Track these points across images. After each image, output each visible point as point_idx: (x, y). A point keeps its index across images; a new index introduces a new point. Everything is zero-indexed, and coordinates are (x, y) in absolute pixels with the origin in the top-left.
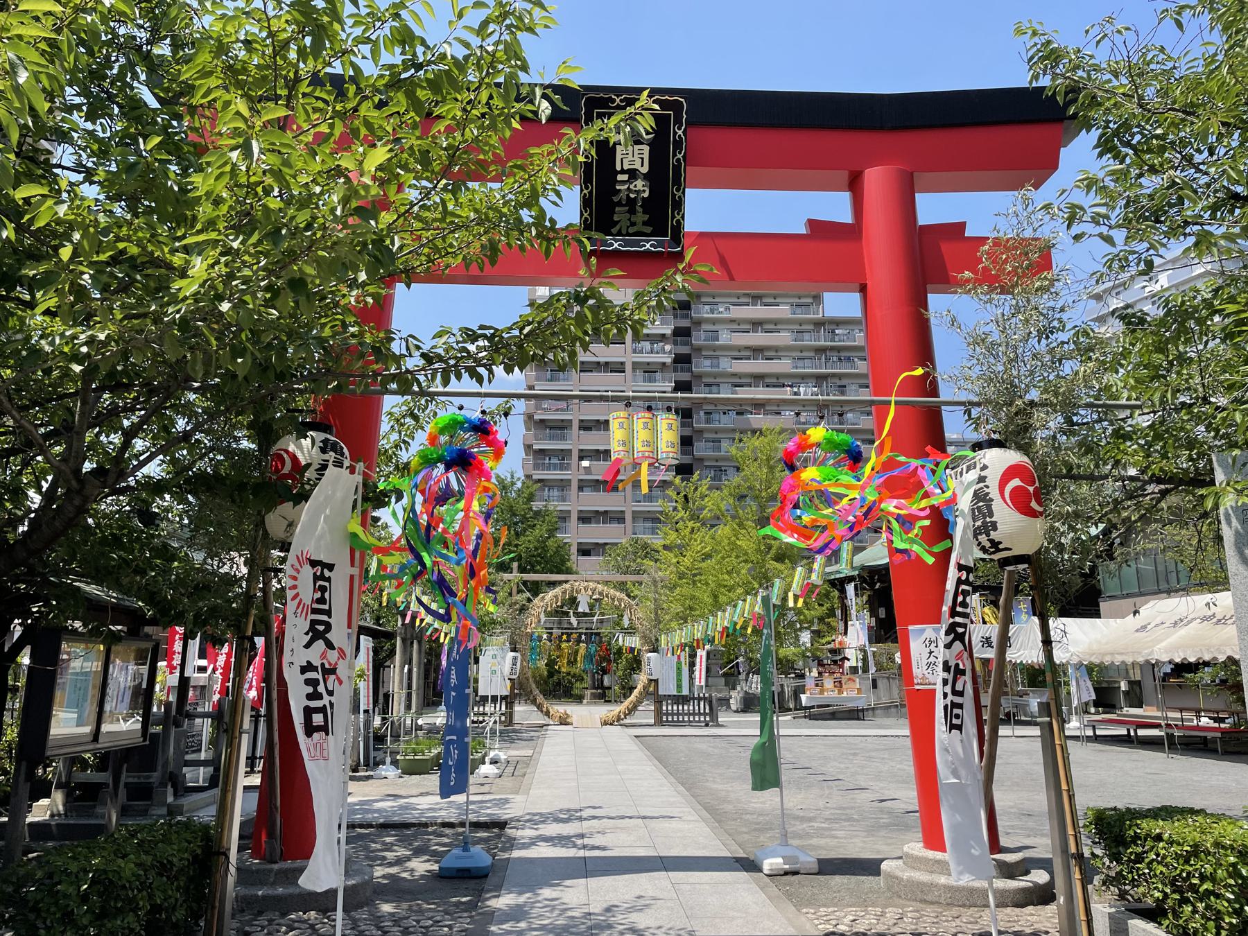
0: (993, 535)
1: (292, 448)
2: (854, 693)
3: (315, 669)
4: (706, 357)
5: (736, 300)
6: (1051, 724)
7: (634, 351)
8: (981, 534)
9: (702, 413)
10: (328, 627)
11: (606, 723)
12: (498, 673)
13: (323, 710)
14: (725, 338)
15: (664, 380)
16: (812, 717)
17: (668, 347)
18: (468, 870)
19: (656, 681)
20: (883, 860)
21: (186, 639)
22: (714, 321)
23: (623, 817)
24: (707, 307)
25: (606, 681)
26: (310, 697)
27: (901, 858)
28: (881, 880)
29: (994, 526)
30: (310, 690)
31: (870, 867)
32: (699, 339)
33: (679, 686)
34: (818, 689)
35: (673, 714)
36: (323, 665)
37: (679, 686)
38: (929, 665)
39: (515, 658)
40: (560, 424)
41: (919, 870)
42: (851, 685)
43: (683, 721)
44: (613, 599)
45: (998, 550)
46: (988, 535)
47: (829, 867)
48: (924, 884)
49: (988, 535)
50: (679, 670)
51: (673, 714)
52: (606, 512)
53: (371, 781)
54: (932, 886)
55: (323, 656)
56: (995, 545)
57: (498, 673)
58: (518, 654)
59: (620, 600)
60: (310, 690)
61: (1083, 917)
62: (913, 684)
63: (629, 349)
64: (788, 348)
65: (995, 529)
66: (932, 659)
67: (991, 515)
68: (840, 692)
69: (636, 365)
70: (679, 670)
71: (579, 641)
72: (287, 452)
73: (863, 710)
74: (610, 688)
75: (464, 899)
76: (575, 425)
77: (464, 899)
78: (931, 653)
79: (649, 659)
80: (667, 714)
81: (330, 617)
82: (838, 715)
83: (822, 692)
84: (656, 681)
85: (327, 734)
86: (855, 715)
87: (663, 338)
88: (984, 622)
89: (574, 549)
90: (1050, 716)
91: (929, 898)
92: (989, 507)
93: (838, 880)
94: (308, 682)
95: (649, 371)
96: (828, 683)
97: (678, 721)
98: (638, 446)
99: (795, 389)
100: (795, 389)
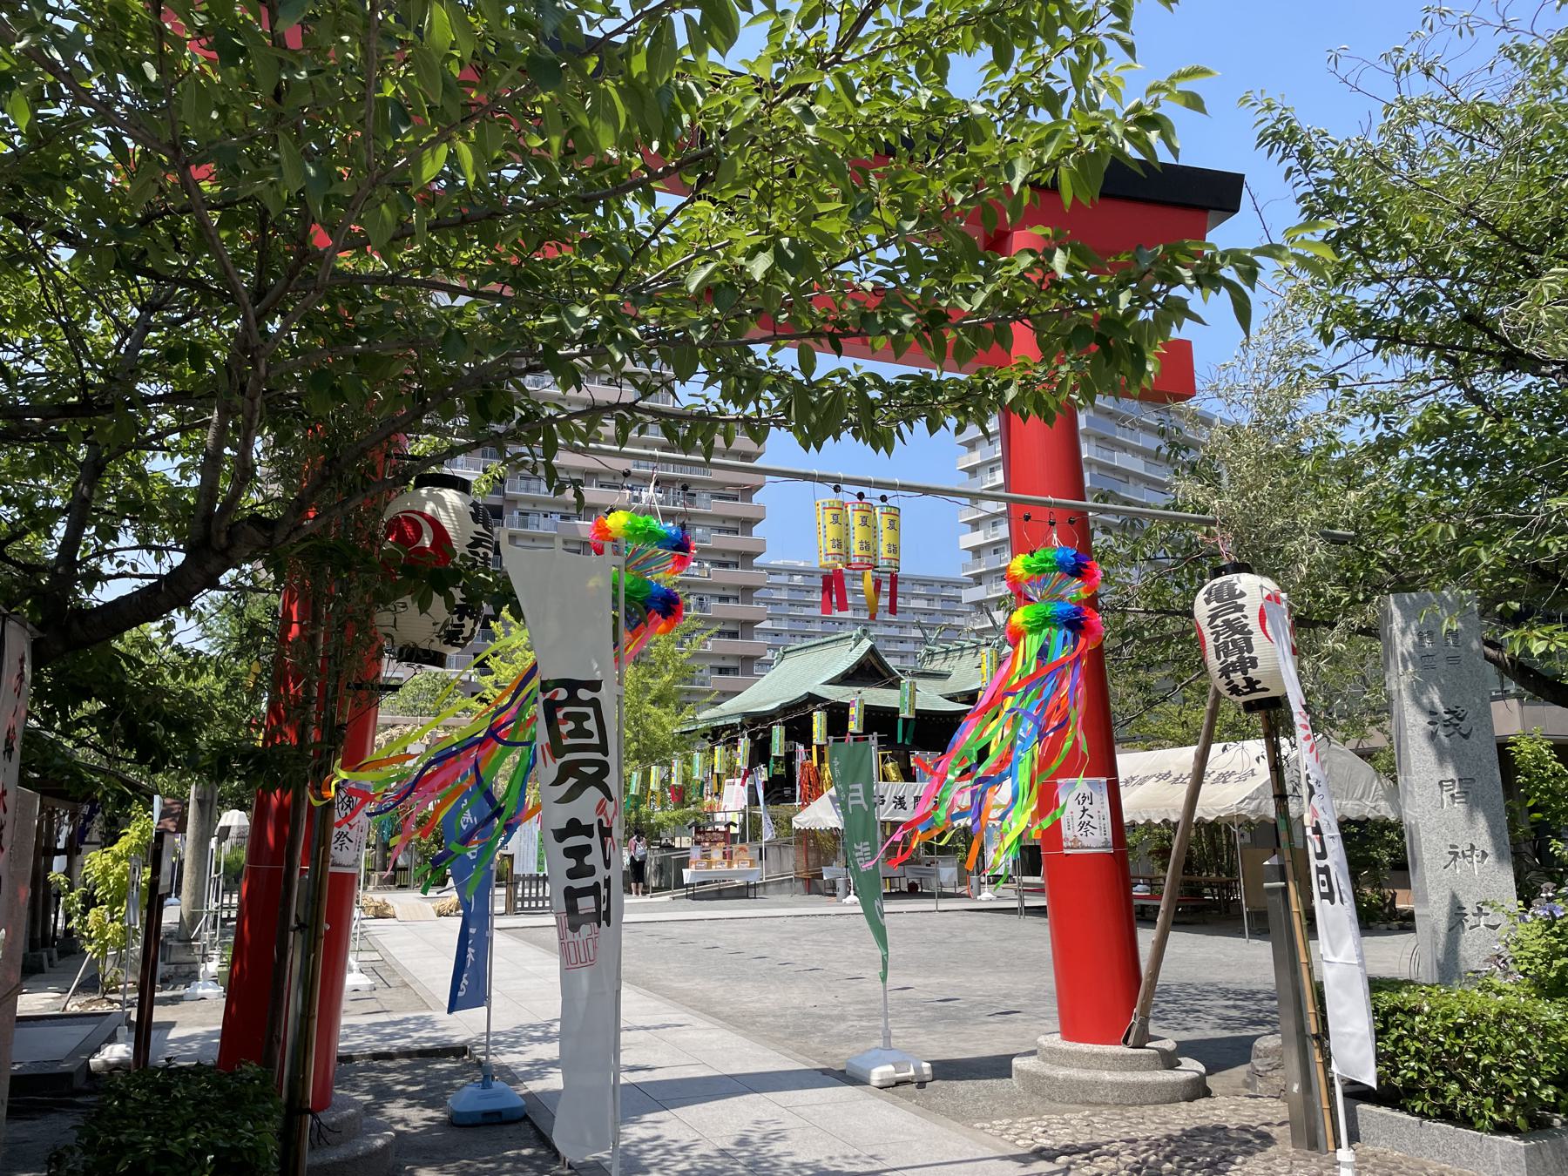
0: (1251, 673)
1: (429, 508)
2: (743, 868)
3: (588, 831)
6: (1285, 890)
8: (1235, 671)
9: (516, 514)
10: (604, 768)
11: (440, 914)
13: (594, 890)
15: (468, 465)
16: (694, 897)
18: (498, 1113)
19: (511, 857)
20: (1013, 1056)
23: (665, 1026)
26: (572, 874)
27: (1033, 1053)
28: (1014, 1082)
29: (1254, 662)
30: (572, 863)
31: (999, 1067)
34: (705, 862)
35: (530, 899)
36: (600, 822)
38: (1082, 825)
41: (1071, 1066)
42: (742, 855)
43: (544, 907)
45: (1254, 690)
46: (1245, 673)
47: (947, 1070)
48: (1086, 1083)
49: (1245, 673)
51: (530, 899)
53: (183, 1005)
54: (1096, 1084)
55: (601, 808)
56: (1252, 684)
60: (572, 863)
61: (1326, 1106)
62: (1062, 848)
65: (1254, 665)
66: (1086, 818)
67: (1250, 650)
68: (730, 865)
72: (422, 514)
73: (755, 886)
75: (526, 1152)
77: (526, 1152)
78: (1084, 811)
80: (523, 899)
81: (606, 754)
82: (725, 894)
83: (709, 865)
84: (511, 857)
85: (1332, 902)
86: (743, 892)
88: (885, 779)
90: (1284, 879)
91: (1094, 1098)
92: (1248, 641)
93: (962, 1086)
94: (569, 852)
96: (716, 854)
97: (537, 908)
98: (855, 547)
99: (636, 493)
100: (636, 493)
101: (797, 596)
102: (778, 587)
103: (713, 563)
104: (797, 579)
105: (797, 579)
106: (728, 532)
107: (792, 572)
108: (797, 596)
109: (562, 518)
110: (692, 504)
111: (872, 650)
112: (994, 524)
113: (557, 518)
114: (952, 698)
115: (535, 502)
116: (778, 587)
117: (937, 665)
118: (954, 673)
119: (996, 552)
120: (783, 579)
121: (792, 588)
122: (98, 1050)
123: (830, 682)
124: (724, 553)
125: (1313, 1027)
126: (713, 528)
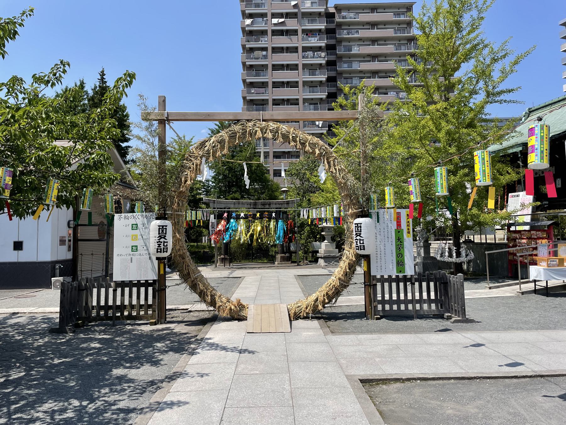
4: (345, 62)
5: (362, 27)
7: (303, 57)
12: (142, 250)
14: (355, 50)
17: (323, 54)
21: (240, 239)
22: (349, 40)
24: (345, 31)
25: (292, 248)
32: (340, 51)
33: (400, 264)
37: (400, 264)
39: (162, 230)
40: (262, 102)
44: (303, 144)
50: (399, 241)
52: (289, 152)
57: (142, 250)
58: (167, 223)
59: (313, 145)
63: (300, 56)
64: (392, 55)
69: (305, 66)
70: (399, 241)
71: (270, 218)
74: (295, 252)
76: (270, 102)
79: (358, 226)
82: (400, 259)
87: (320, 49)
89: (272, 173)
95: (311, 68)
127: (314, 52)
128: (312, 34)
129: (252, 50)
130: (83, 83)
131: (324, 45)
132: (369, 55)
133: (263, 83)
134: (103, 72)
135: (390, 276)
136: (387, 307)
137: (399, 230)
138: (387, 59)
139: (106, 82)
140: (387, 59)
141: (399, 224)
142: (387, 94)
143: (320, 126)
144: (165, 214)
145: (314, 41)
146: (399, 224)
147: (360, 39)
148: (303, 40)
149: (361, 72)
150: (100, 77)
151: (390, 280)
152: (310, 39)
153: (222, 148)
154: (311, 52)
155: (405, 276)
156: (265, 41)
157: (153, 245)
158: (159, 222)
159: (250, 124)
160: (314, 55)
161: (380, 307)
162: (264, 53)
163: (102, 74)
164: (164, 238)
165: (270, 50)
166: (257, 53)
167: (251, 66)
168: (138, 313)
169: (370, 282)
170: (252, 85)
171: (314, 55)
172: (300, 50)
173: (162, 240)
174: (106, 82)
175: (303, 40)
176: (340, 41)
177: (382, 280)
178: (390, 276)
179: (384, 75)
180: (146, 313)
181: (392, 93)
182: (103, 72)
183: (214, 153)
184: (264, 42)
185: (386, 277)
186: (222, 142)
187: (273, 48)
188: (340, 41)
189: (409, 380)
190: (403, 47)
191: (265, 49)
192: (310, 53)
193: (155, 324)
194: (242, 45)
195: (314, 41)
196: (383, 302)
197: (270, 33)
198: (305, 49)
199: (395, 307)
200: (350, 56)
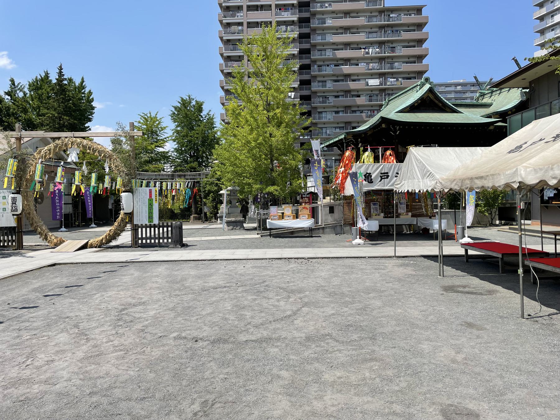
4: (319, 34)
9: (316, 66)
14: (330, 22)
22: (323, 13)
24: (319, 5)
32: (315, 23)
33: (151, 218)
37: (151, 218)
39: (14, 200)
64: (364, 27)
87: (293, 23)
99: (367, 50)
101: (459, 95)
102: (450, 92)
103: (404, 78)
104: (459, 88)
105: (459, 88)
106: (411, 63)
107: (456, 85)
108: (459, 95)
109: (335, 66)
110: (393, 52)
111: (431, 90)
112: (552, 16)
113: (333, 66)
114: (489, 116)
115: (324, 60)
116: (450, 92)
117: (486, 100)
118: (494, 103)
119: (552, 30)
120: (452, 88)
121: (456, 92)
122: (111, 242)
123: (401, 111)
124: (409, 73)
125: (108, 268)
126: (403, 62)
127: (287, 26)
128: (285, 9)
129: (229, 25)
130: (48, 74)
131: (295, 19)
132: (341, 28)
133: (240, 56)
134: (61, 67)
135: (146, 225)
136: (144, 241)
137: (150, 199)
138: (359, 30)
139: (64, 75)
140: (359, 30)
141: (151, 196)
142: (358, 65)
143: (293, 97)
144: (20, 191)
145: (287, 16)
146: (151, 196)
147: (333, 12)
148: (276, 14)
149: (334, 44)
150: (58, 71)
151: (146, 227)
152: (283, 13)
153: (50, 154)
154: (284, 26)
155: (154, 224)
156: (241, 16)
157: (9, 207)
158: (13, 195)
159: (67, 140)
160: (286, 29)
161: (140, 241)
162: (240, 28)
163: (61, 69)
164: (15, 204)
165: (245, 25)
166: (233, 28)
167: (229, 41)
168: (8, 244)
169: (135, 229)
170: (228, 59)
171: (286, 29)
172: (274, 24)
173: (14, 205)
174: (64, 75)
175: (276, 14)
176: (314, 14)
177: (142, 227)
178: (146, 225)
179: (356, 46)
180: (12, 244)
181: (362, 64)
182: (61, 67)
183: (45, 156)
184: (240, 17)
185: (144, 225)
186: (50, 150)
187: (249, 23)
188: (314, 14)
189: (77, 263)
190: (375, 19)
191: (240, 24)
192: (284, 28)
193: (16, 250)
194: (219, 21)
195: (287, 16)
196: (142, 239)
197: (245, 8)
198: (279, 23)
199: (148, 241)
200: (323, 29)
